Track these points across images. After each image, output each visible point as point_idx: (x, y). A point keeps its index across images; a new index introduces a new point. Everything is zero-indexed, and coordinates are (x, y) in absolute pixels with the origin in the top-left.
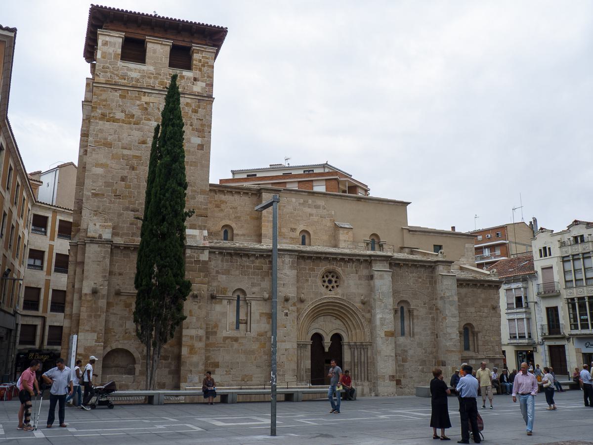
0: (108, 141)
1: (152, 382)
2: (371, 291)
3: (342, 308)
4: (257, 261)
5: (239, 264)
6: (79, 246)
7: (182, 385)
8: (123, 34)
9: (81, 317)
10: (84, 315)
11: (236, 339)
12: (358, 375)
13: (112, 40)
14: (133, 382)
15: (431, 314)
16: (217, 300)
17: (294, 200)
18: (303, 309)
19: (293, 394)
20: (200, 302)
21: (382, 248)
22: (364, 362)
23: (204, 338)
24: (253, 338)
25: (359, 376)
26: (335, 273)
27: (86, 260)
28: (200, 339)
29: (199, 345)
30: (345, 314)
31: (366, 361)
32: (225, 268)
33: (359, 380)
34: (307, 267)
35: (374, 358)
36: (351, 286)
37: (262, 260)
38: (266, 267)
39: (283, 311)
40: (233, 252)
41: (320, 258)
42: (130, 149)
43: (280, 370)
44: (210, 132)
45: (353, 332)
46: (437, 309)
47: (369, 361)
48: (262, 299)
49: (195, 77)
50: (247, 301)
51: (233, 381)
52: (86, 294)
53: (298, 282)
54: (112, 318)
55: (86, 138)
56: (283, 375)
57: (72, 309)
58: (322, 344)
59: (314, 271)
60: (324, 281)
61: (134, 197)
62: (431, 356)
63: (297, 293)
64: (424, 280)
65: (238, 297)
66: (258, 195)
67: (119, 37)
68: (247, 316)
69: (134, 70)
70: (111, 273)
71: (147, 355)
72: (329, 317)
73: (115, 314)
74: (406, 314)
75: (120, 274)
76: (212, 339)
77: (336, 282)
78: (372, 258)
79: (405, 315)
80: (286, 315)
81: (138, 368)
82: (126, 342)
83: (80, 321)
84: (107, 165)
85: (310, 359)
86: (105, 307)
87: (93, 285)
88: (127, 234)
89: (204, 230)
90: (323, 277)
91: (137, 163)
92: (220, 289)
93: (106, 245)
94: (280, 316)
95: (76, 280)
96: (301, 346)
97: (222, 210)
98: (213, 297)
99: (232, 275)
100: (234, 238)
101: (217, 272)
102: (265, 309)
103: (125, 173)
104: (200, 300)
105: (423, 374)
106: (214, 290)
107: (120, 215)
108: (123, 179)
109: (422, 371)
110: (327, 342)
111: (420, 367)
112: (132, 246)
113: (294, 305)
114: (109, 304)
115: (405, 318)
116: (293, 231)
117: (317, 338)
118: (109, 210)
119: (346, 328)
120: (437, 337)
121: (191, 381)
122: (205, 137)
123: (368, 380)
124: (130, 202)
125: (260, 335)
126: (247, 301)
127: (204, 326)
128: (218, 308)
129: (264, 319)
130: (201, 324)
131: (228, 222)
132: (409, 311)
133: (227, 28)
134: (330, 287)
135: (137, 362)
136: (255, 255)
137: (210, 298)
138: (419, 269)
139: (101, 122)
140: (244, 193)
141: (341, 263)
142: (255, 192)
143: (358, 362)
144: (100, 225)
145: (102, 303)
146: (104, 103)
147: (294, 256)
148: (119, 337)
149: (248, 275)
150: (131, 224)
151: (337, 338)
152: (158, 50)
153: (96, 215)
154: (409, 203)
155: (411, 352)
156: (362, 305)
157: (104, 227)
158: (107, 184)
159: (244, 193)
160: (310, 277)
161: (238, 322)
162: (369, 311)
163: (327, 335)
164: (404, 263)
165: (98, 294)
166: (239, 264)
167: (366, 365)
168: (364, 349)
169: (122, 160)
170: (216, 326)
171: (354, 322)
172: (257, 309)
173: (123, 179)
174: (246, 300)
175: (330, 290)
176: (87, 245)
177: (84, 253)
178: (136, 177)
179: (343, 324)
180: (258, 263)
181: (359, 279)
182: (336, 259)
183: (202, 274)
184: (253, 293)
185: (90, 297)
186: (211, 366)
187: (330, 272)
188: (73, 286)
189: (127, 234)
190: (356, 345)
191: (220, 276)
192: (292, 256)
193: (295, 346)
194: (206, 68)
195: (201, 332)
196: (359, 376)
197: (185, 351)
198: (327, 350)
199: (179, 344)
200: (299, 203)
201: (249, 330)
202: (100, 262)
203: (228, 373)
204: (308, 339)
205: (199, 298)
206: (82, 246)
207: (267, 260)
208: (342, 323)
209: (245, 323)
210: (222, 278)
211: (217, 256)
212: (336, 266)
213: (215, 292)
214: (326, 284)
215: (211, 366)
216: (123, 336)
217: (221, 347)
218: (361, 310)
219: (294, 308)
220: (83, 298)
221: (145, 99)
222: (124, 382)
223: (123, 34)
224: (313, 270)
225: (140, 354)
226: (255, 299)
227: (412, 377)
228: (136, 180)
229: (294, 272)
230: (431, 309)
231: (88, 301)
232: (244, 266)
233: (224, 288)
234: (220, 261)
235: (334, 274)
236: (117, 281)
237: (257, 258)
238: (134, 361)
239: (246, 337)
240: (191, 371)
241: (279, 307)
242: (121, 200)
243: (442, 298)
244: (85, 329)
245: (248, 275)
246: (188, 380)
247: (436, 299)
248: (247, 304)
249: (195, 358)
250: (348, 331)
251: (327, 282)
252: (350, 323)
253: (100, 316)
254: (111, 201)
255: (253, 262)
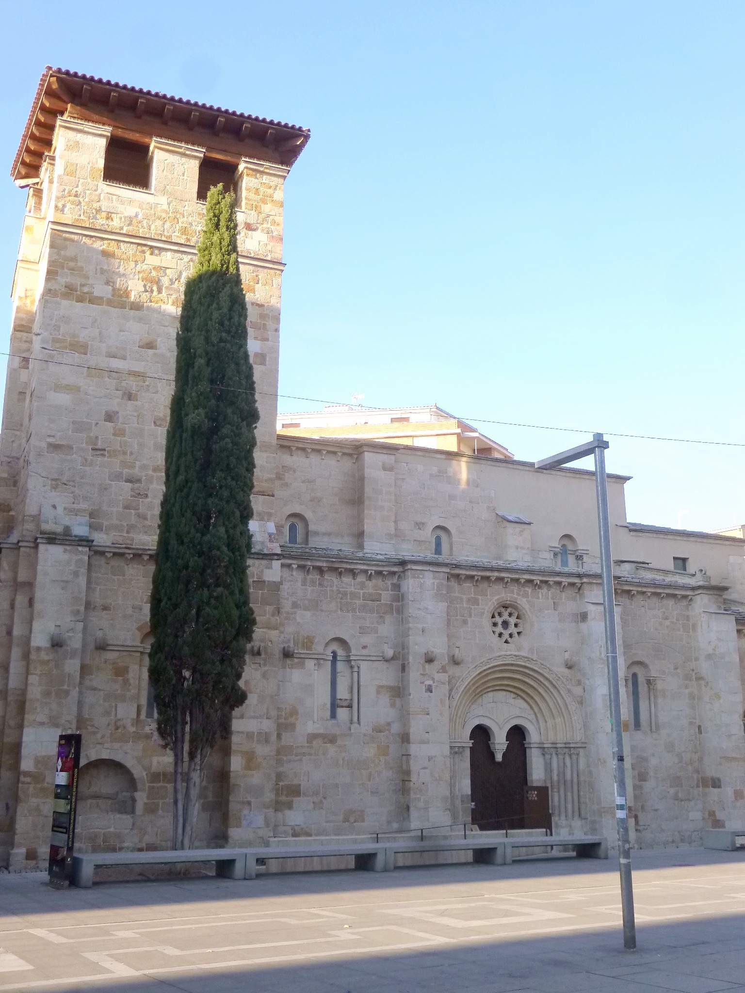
0: (81, 340)
1: (188, 828)
2: (582, 644)
3: (528, 675)
4: (370, 584)
5: (335, 588)
6: (22, 549)
7: (234, 833)
8: (107, 130)
9: (29, 696)
10: (35, 691)
11: (331, 739)
12: (559, 807)
13: (90, 139)
14: (132, 829)
15: (687, 687)
16: (296, 660)
17: (420, 468)
18: (459, 678)
19: (496, 848)
20: (265, 665)
21: (580, 562)
22: (572, 781)
23: (274, 738)
24: (365, 735)
25: (563, 809)
26: (516, 608)
27: (40, 578)
28: (265, 738)
29: (262, 751)
30: (533, 687)
31: (575, 780)
32: (309, 597)
33: (563, 817)
34: (464, 597)
35: (590, 772)
36: (547, 632)
37: (378, 582)
38: (386, 596)
39: (423, 683)
40: (325, 565)
41: (488, 578)
42: (124, 358)
43: (419, 799)
44: (277, 330)
45: (550, 723)
46: (699, 678)
47: (582, 778)
48: (381, 659)
49: (248, 221)
50: (353, 663)
51: (327, 822)
52: (38, 649)
53: (448, 625)
54: (90, 698)
55: (25, 334)
56: (426, 809)
57: (7, 678)
58: (489, 747)
59: (478, 605)
60: (495, 624)
61: (131, 453)
62: (690, 768)
63: (449, 647)
64: (672, 622)
65: (335, 654)
66: (355, 456)
67: (101, 136)
68: (351, 692)
69: (125, 200)
70: (88, 605)
71: (176, 771)
72: (504, 693)
73: (95, 689)
74: (643, 688)
75: (105, 608)
76: (287, 739)
77: (516, 625)
78: (585, 580)
79: (640, 688)
80: (429, 689)
81: (141, 797)
82: (117, 745)
83: (27, 704)
84: (78, 389)
85: (469, 777)
86: (78, 674)
87: (51, 628)
88: (118, 528)
89: (269, 520)
90: (493, 617)
91: (137, 386)
92: (300, 638)
93: (80, 549)
94: (416, 691)
95: (16, 620)
96: (455, 751)
97: (286, 485)
98: (287, 654)
99: (322, 611)
100: (310, 539)
101: (295, 605)
102: (387, 676)
103: (115, 404)
104: (265, 660)
105: (676, 802)
106: (289, 640)
107: (104, 489)
108: (110, 417)
109: (676, 798)
110: (500, 743)
111: (672, 791)
112: (129, 551)
113: (444, 670)
114: (84, 670)
115: (640, 696)
116: (420, 529)
117: (481, 734)
118: (82, 478)
119: (535, 714)
120: (700, 732)
121: (251, 823)
122: (267, 340)
123: (580, 815)
124: (123, 464)
125: (378, 730)
126: (353, 663)
127: (273, 713)
128: (296, 676)
129: (385, 699)
130: (268, 709)
131: (298, 509)
132: (649, 682)
133: (309, 130)
134: (506, 634)
135: (139, 786)
136: (366, 571)
137: (282, 655)
138: (665, 602)
139: (65, 303)
140: (329, 452)
141: (527, 589)
142: (350, 451)
143: (559, 781)
144: (65, 509)
145: (72, 666)
146: (72, 264)
147: (442, 574)
148: (103, 737)
149: (354, 610)
150: (126, 507)
151: (517, 734)
152: (174, 166)
153: (55, 488)
154: (629, 478)
155: (654, 761)
156: (567, 671)
157: (71, 511)
158: (79, 427)
159: (329, 452)
160: (470, 616)
161: (334, 706)
162: (579, 683)
163: (500, 729)
164: (640, 589)
165: (65, 648)
166: (335, 588)
167: (575, 788)
168: (570, 755)
169: (107, 379)
170: (294, 712)
171: (551, 704)
172: (374, 677)
173: (110, 417)
174: (349, 661)
175: (506, 642)
176: (41, 547)
177: (33, 566)
178: (136, 414)
179: (528, 707)
180: (371, 586)
181: (560, 621)
182: (517, 580)
183: (268, 608)
184: (364, 647)
185: (47, 654)
186: (285, 793)
187: (505, 607)
188: (9, 633)
189: (118, 528)
190: (556, 748)
191: (299, 612)
192: (437, 574)
193: (447, 751)
194: (269, 205)
195: (267, 725)
196: (563, 809)
197: (236, 763)
198: (499, 757)
199: (226, 752)
200: (431, 475)
201: (355, 719)
202: (67, 582)
203: (317, 805)
204: (465, 738)
205: (263, 656)
206: (28, 550)
207: (389, 583)
208: (525, 705)
209: (348, 707)
210: (304, 617)
211: (294, 573)
212: (518, 594)
213: (292, 645)
214: (499, 629)
215: (285, 793)
216: (111, 734)
217: (304, 754)
218: (565, 680)
219: (444, 677)
220: (33, 656)
221: (152, 260)
222: (112, 830)
223: (107, 130)
224: (476, 602)
225: (146, 770)
226: (367, 659)
227: (656, 810)
228: (135, 419)
229: (443, 606)
230: (687, 677)
231: (44, 663)
232: (345, 594)
233: (308, 637)
234: (299, 584)
235: (513, 611)
236: (101, 624)
237: (370, 578)
238: (132, 783)
239: (351, 735)
240: (249, 803)
241: (414, 675)
242: (106, 459)
243: (709, 657)
244: (38, 719)
245: (354, 610)
246: (244, 823)
247: (697, 659)
248: (352, 667)
249: (256, 778)
250: (537, 720)
251: (500, 626)
252: (542, 705)
253: (67, 693)
254: (86, 460)
255: (362, 586)
